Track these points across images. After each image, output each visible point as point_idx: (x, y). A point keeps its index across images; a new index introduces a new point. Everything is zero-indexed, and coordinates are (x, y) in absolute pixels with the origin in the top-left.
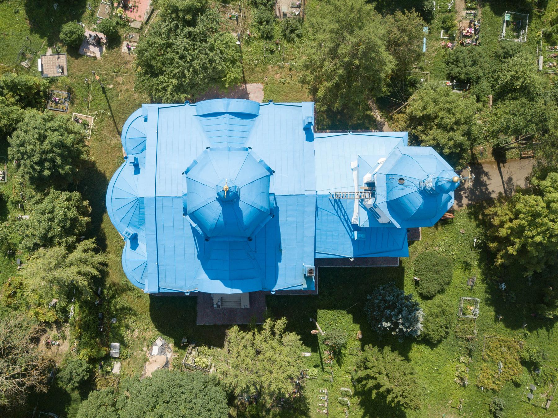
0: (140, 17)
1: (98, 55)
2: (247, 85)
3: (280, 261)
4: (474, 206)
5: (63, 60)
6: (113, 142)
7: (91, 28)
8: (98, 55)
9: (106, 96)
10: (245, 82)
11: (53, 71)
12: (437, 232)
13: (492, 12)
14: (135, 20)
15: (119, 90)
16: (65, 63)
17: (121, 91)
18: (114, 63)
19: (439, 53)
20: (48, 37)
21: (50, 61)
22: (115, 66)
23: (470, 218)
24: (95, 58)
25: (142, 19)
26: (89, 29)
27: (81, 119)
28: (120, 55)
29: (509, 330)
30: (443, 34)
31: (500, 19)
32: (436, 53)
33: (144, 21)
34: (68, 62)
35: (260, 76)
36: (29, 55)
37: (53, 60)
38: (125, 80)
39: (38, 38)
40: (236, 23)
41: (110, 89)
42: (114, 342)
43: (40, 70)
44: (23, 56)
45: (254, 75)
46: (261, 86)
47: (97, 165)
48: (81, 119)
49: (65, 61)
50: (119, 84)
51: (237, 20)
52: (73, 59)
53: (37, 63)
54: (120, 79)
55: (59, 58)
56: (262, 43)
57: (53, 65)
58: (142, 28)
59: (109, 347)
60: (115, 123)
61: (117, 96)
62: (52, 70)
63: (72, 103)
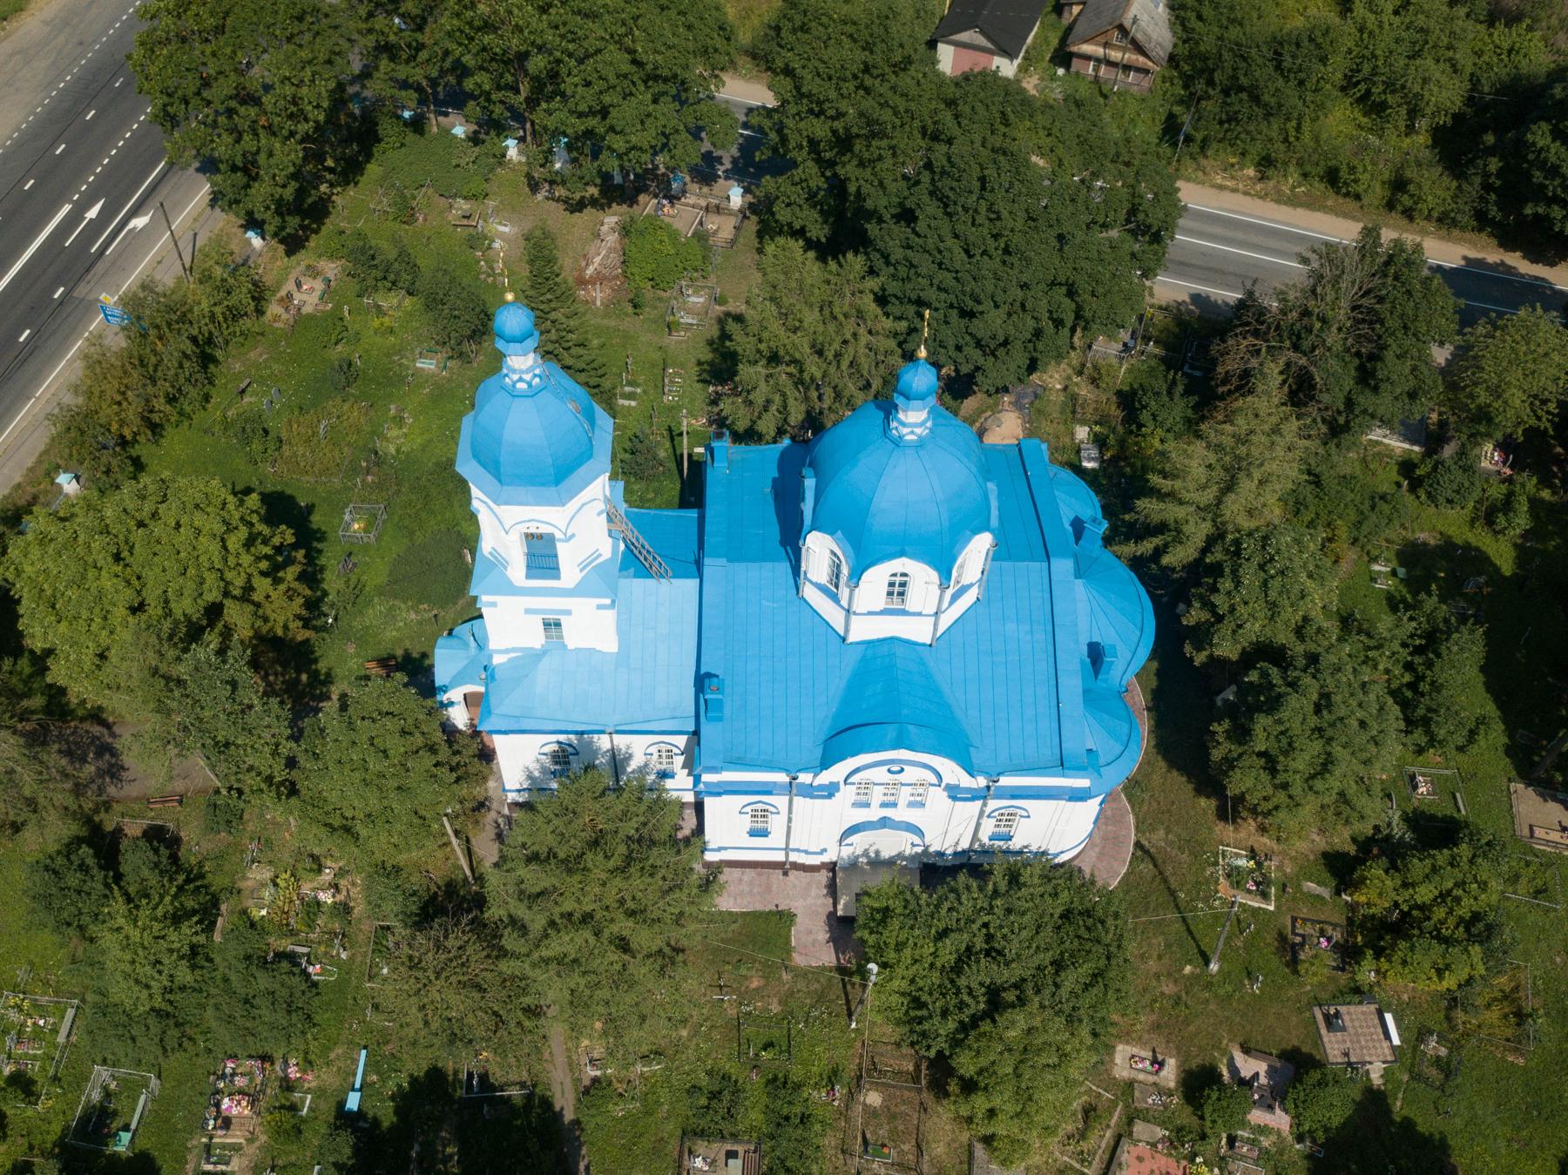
0: (1140, 1159)
1: (1240, 1058)
2: (834, 962)
3: (774, 480)
4: (314, 698)
5: (1333, 1047)
6: (1162, 833)
7: (1273, 1138)
8: (1240, 1058)
9: (1198, 946)
10: (841, 970)
11: (1352, 1021)
12: (408, 645)
13: (159, 1162)
14: (1154, 1145)
15: (1166, 960)
16: (1326, 1040)
17: (1160, 957)
18: (1192, 1028)
19: (326, 1050)
20: (1392, 1122)
21: (1368, 1048)
22: (1187, 1022)
23: (328, 675)
24: (1246, 1050)
25: (1135, 1151)
26: (1279, 1133)
27: (1249, 891)
28: (1178, 1049)
29: (289, 492)
30: (303, 1103)
31: (144, 1144)
32: (332, 1056)
33: (1125, 1145)
34: (1318, 1040)
35: (801, 985)
36: (1434, 1073)
37: (1362, 1048)
38: (1154, 983)
39: (1419, 1120)
40: (868, 1136)
41: (1190, 962)
42: (1093, 470)
43: (1389, 1017)
44: (1446, 1068)
45: (816, 986)
46: (799, 960)
47: (1191, 786)
48: (1249, 891)
49: (1328, 1046)
50: (1169, 975)
51: (865, 1142)
52: (1305, 1049)
53: (1400, 1036)
54: (1169, 988)
55: (1346, 1054)
56: (797, 1072)
57: (1356, 1034)
58: (1130, 1122)
59: (1102, 461)
60: (1165, 880)
61: (1168, 946)
62: (1357, 1024)
63: (1282, 938)
